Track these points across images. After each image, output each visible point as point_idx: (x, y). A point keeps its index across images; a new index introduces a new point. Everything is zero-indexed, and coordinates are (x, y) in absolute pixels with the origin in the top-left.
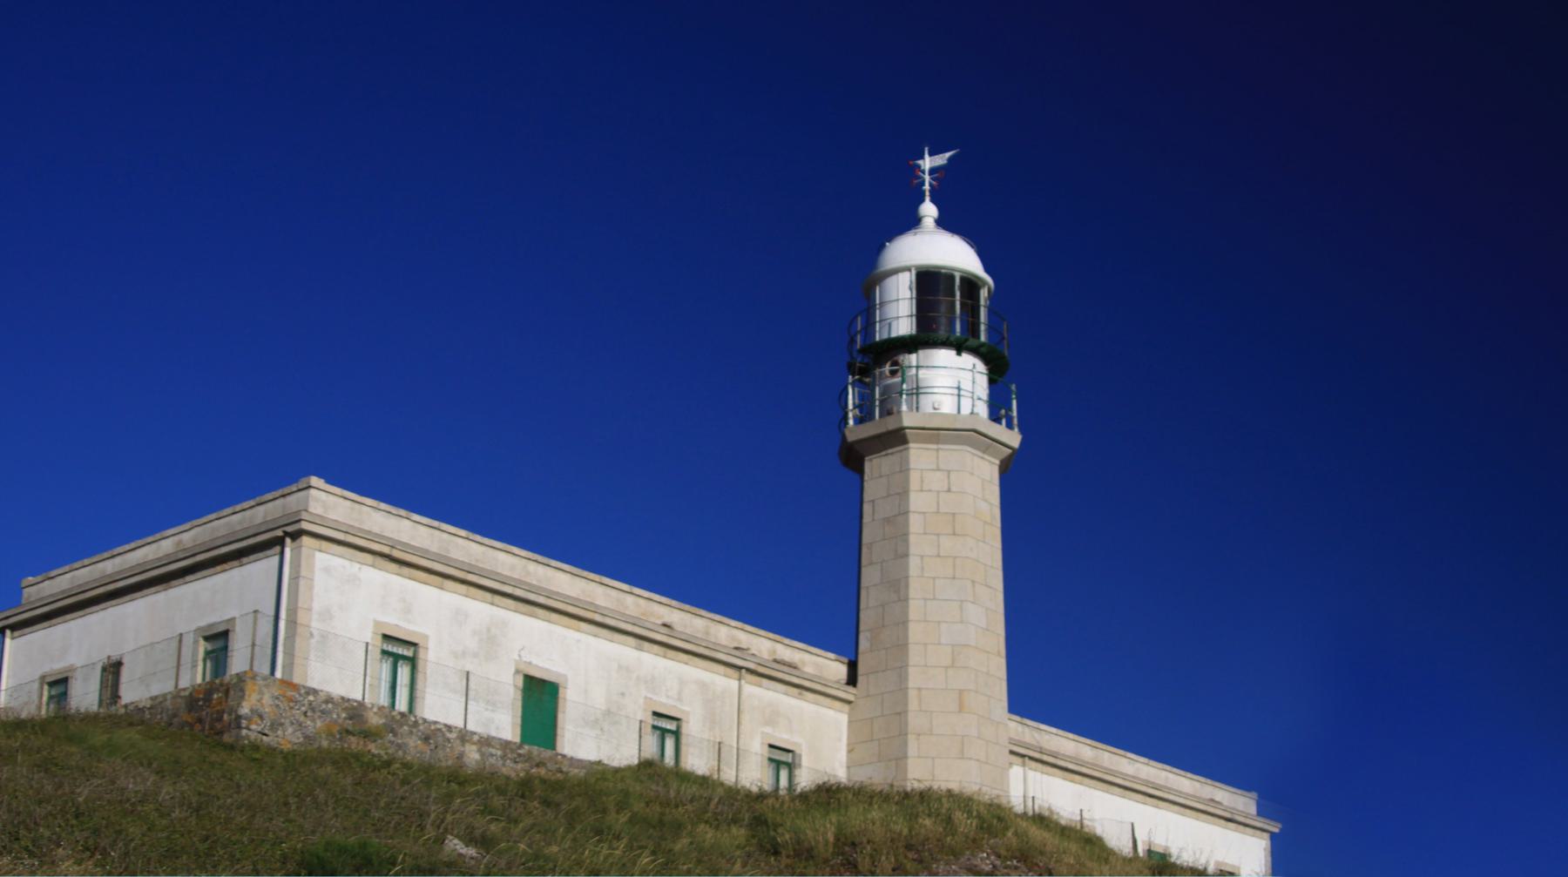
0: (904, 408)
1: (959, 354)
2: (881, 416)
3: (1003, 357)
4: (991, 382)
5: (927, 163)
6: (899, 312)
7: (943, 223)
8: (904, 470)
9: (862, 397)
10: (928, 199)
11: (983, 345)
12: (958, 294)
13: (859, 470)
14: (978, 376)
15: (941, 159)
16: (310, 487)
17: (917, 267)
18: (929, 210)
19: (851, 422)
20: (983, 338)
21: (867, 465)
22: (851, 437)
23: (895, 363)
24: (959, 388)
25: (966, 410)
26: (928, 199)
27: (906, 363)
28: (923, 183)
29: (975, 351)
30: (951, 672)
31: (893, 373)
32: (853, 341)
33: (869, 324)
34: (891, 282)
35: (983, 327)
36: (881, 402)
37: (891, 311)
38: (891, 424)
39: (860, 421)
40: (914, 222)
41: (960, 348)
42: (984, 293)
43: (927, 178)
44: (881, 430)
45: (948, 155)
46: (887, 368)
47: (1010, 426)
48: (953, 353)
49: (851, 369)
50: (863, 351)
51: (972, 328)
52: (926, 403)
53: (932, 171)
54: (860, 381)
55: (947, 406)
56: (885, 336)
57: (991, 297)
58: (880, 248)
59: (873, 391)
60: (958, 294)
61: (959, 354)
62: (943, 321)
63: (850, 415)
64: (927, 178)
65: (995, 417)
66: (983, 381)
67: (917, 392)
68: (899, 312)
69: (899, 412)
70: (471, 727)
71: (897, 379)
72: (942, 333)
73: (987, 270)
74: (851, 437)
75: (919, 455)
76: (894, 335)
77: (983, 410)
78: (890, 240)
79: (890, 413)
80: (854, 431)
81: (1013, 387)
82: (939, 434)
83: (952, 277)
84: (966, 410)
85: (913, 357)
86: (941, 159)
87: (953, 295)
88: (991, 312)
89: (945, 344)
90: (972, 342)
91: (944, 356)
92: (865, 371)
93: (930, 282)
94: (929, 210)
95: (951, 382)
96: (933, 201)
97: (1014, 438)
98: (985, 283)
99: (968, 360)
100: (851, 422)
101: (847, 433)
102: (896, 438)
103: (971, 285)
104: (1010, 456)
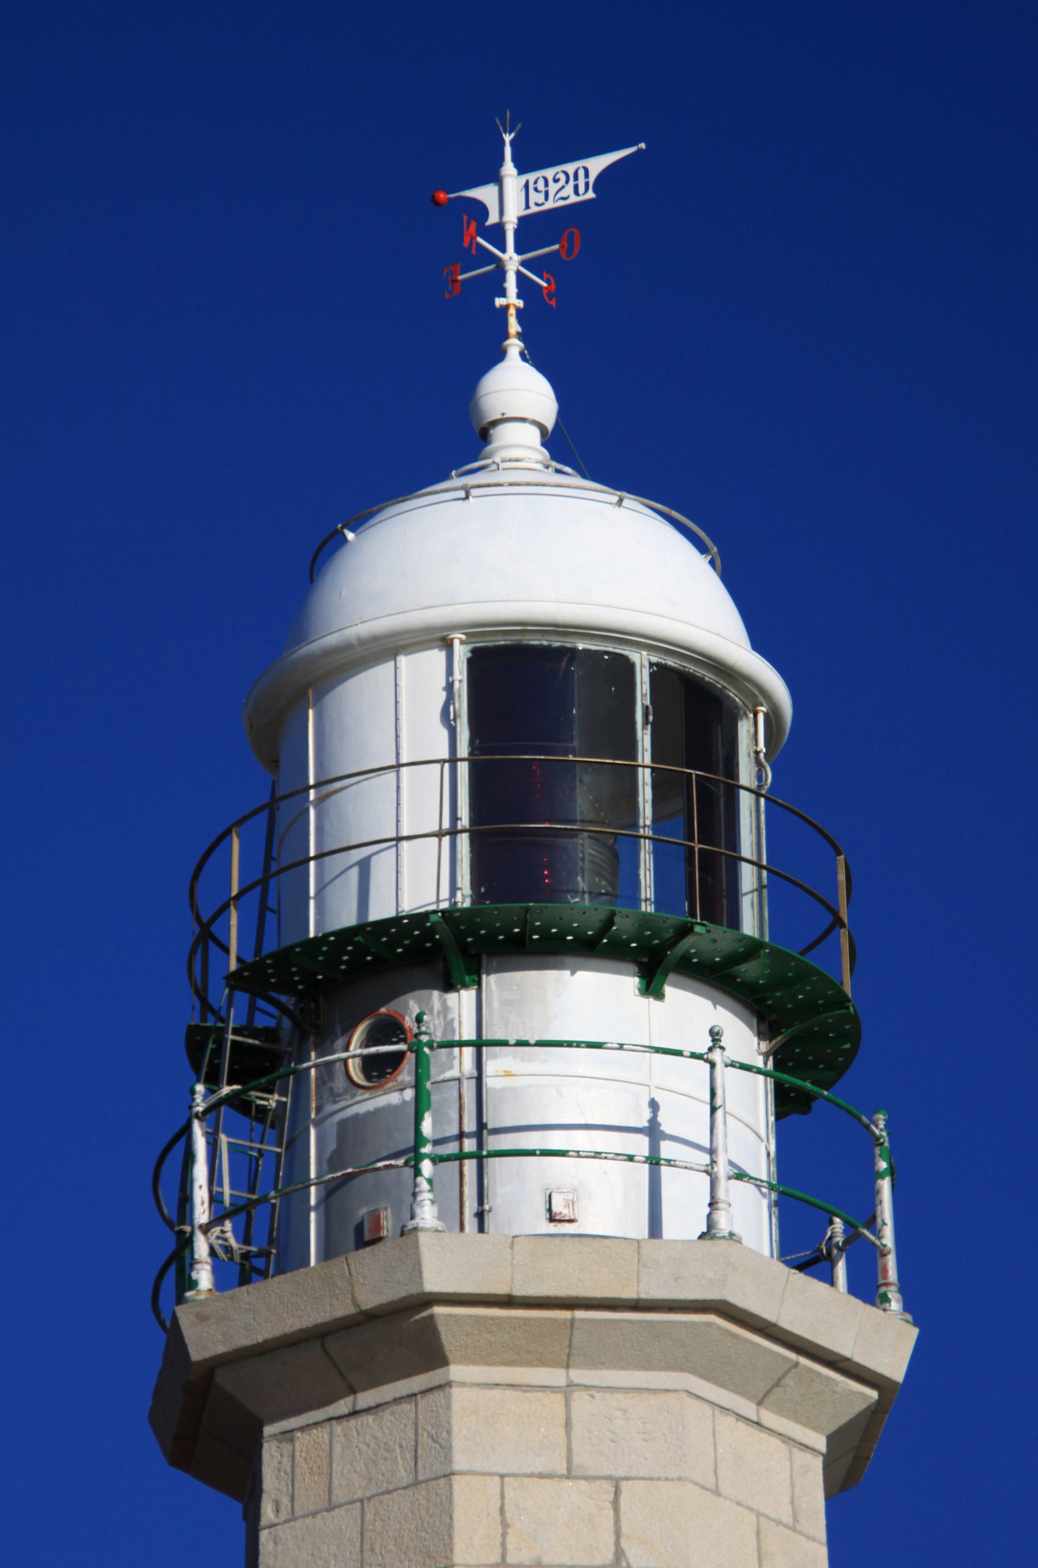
0: (427, 1214)
1: (651, 988)
2: (328, 1252)
3: (842, 1001)
4: (787, 1103)
5: (511, 196)
6: (397, 818)
7: (581, 446)
8: (431, 1477)
9: (247, 1171)
10: (514, 346)
11: (753, 948)
12: (644, 739)
13: (240, 1481)
14: (730, 1080)
15: (569, 183)
16: (449, 1384)
17: (473, 630)
18: (519, 392)
19: (204, 1277)
20: (749, 925)
21: (273, 1458)
22: (204, 1342)
23: (389, 1029)
24: (653, 1131)
25: (683, 1221)
26: (514, 346)
27: (434, 1028)
28: (496, 282)
29: (717, 976)
30: (640, 1145)
31: (380, 1069)
32: (208, 937)
33: (280, 867)
34: (365, 694)
35: (748, 877)
36: (331, 1191)
37: (363, 812)
38: (369, 1282)
39: (240, 1271)
40: (458, 444)
41: (654, 963)
42: (750, 737)
43: (512, 260)
44: (337, 1308)
45: (597, 164)
46: (355, 1048)
47: (866, 1288)
48: (629, 983)
49: (201, 1050)
50: (251, 979)
51: (709, 885)
52: (518, 1191)
53: (533, 230)
54: (239, 1104)
55: (606, 1201)
56: (348, 918)
57: (780, 751)
58: (327, 546)
59: (296, 1146)
60: (644, 739)
61: (651, 988)
62: (585, 850)
63: (201, 1247)
64: (512, 260)
65: (804, 1250)
66: (751, 1100)
67: (479, 1145)
68: (397, 818)
69: (407, 1233)
70: (459, 1485)
71: (395, 1096)
72: (581, 905)
73: (761, 641)
74: (204, 1342)
75: (491, 1415)
76: (380, 910)
77: (752, 1217)
78: (359, 521)
79: (366, 1237)
80: (217, 1317)
81: (880, 1126)
82: (568, 1321)
83: (627, 667)
84: (683, 1221)
85: (462, 1002)
86: (569, 183)
87: (630, 749)
88: (778, 807)
89: (595, 947)
90: (706, 939)
91: (592, 997)
92: (259, 1064)
93: (526, 690)
94: (519, 392)
95: (614, 1105)
96: (534, 356)
97: (885, 1340)
98: (756, 692)
99: (689, 1012)
100: (204, 1277)
101: (185, 1316)
102: (395, 1342)
103: (697, 701)
104: (873, 1413)
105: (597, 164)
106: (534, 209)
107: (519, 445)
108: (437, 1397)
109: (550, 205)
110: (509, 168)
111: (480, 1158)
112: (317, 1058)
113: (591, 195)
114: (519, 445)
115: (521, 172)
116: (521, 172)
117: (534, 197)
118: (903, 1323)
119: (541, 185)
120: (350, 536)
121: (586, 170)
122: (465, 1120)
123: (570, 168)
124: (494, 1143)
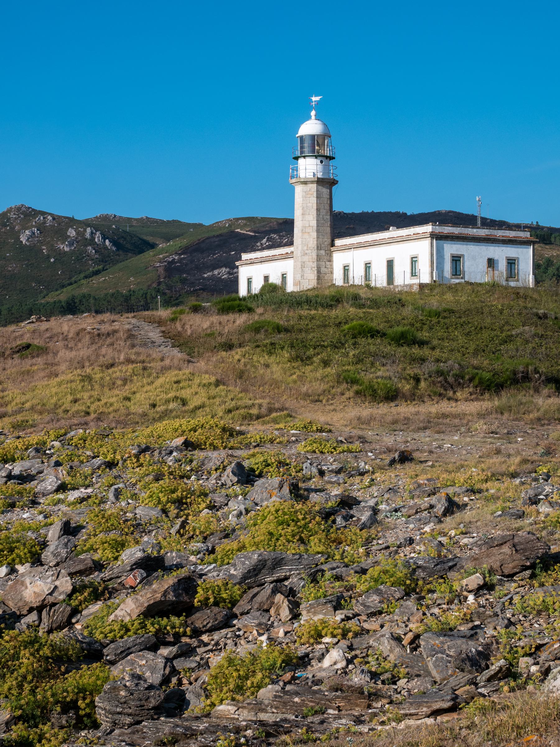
15: (318, 98)
86: (318, 98)
94: (313, 113)
114: (313, 117)
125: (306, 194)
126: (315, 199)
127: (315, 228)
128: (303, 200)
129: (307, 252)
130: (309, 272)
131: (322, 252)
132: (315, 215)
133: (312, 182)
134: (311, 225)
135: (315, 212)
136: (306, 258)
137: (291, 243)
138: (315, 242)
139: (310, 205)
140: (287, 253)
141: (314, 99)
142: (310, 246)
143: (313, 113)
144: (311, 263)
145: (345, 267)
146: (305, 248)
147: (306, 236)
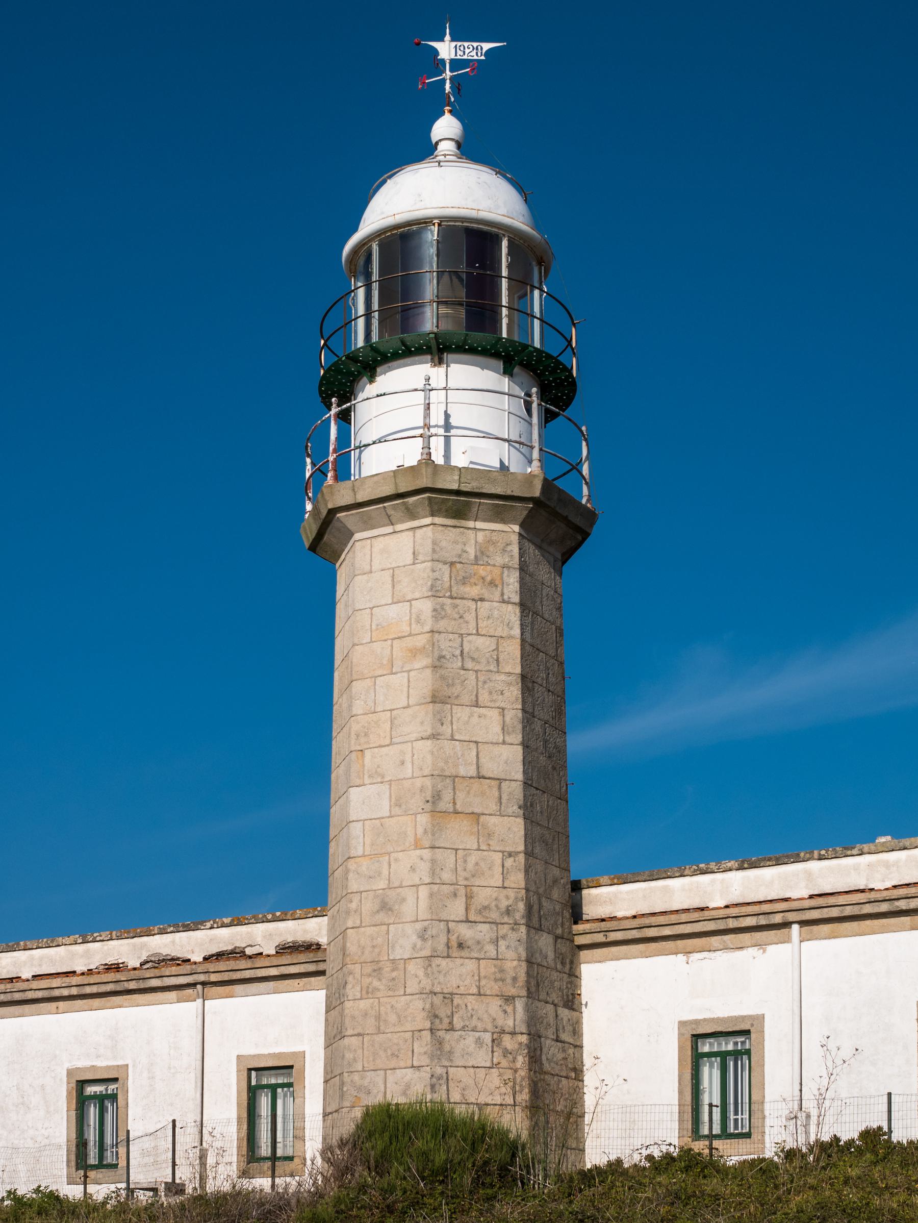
7: (469, 149)
15: (475, 50)
45: (487, 46)
86: (475, 50)
94: (446, 128)
105: (487, 46)
106: (458, 57)
107: (446, 147)
108: (387, 521)
109: (465, 57)
110: (448, 38)
111: (427, 426)
112: (339, 406)
113: (483, 58)
114: (446, 147)
115: (453, 40)
116: (453, 40)
117: (459, 53)
118: (550, 276)
119: (462, 48)
120: (905, 1142)
121: (482, 48)
122: (714, 1126)
123: (475, 44)
124: (453, 432)
125: (450, 587)
126: (513, 614)
127: (515, 790)
128: (438, 613)
129: (466, 932)
130: (482, 1058)
131: (545, 942)
132: (514, 714)
133: (500, 504)
134: (491, 768)
135: (515, 692)
136: (459, 974)
137: (309, 886)
138: (518, 879)
139: (483, 644)
140: (116, 968)
141: (446, 49)
142: (483, 896)
143: (446, 128)
144: (494, 1006)
145: (82, 1084)
146: (457, 909)
147: (458, 833)
